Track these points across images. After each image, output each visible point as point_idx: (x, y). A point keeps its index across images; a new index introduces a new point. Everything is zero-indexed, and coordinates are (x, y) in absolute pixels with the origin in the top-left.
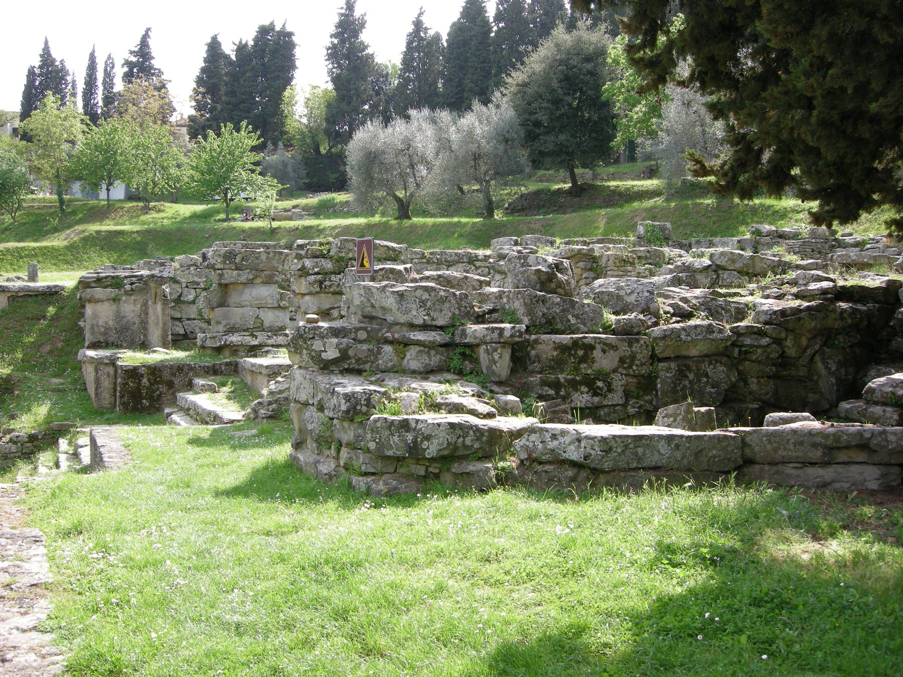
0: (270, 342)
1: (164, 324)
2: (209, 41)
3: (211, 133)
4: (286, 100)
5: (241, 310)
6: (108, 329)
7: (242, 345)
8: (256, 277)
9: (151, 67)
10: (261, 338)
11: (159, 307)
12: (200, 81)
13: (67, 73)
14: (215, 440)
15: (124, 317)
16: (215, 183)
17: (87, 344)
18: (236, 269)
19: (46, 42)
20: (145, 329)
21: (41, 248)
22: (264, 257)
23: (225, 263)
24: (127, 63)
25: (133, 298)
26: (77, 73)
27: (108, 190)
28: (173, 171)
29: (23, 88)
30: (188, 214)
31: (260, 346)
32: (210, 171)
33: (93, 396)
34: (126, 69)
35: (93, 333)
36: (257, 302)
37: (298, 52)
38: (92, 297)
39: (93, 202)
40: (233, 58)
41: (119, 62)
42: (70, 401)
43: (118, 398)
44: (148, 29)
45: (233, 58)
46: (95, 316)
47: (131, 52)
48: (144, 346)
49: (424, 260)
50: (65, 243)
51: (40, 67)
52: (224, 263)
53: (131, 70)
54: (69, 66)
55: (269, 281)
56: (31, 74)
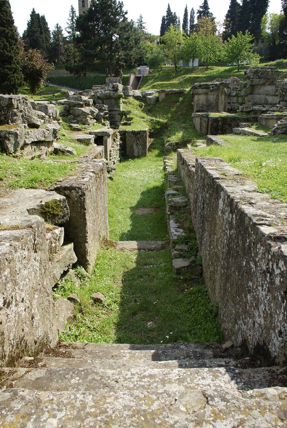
0: (270, 109)
1: (225, 104)
3: (233, 36)
4: (263, 21)
5: (259, 96)
7: (259, 110)
8: (266, 82)
9: (208, 12)
10: (267, 107)
11: (223, 96)
12: (227, 16)
13: (177, 18)
14: (258, 140)
16: (235, 56)
17: (195, 111)
19: (169, 6)
20: (217, 105)
21: (169, 84)
22: (270, 73)
26: (180, 16)
27: (193, 62)
28: (218, 53)
29: (161, 25)
30: (223, 70)
34: (198, 14)
35: (197, 107)
38: (198, 92)
39: (187, 67)
40: (241, 5)
41: (196, 11)
43: (209, 130)
45: (241, 5)
46: (199, 100)
47: (200, 7)
48: (218, 111)
50: (178, 82)
51: (167, 16)
53: (200, 15)
54: (177, 15)
55: (272, 84)
56: (163, 19)
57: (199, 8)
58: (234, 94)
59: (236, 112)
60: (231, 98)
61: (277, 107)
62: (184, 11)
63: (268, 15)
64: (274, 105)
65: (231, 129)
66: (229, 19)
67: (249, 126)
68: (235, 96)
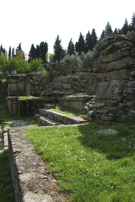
1: (31, 90)
2: (32, 45)
5: (57, 83)
6: (14, 91)
7: (58, 94)
9: (21, 50)
11: (29, 85)
12: (30, 52)
13: (5, 51)
15: (19, 88)
16: (35, 69)
17: (8, 95)
18: (56, 70)
19: (1, 45)
22: (64, 67)
23: (53, 68)
24: (16, 49)
25: (22, 82)
26: (7, 50)
27: (13, 71)
31: (63, 94)
32: (33, 67)
33: (10, 110)
35: (10, 92)
36: (62, 81)
37: (48, 47)
41: (15, 49)
42: (3, 112)
44: (20, 43)
45: (36, 48)
46: (11, 87)
47: (17, 47)
48: (26, 96)
49: (94, 76)
52: (52, 68)
54: (6, 50)
57: (16, 48)
58: (37, 84)
59: (39, 96)
60: (35, 86)
61: (71, 91)
62: (9, 48)
63: (48, 54)
64: (68, 90)
65: (37, 109)
66: (31, 53)
67: (54, 108)
68: (38, 85)
